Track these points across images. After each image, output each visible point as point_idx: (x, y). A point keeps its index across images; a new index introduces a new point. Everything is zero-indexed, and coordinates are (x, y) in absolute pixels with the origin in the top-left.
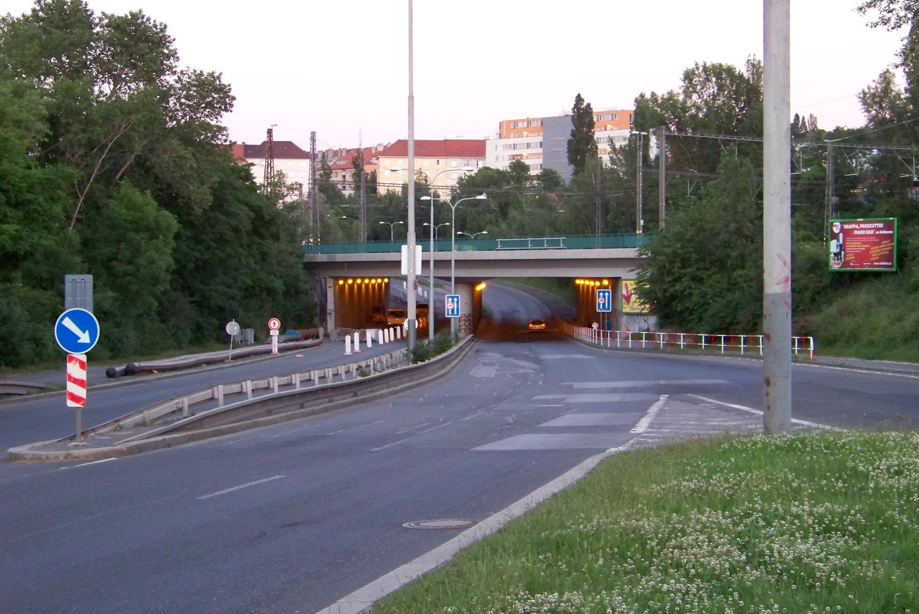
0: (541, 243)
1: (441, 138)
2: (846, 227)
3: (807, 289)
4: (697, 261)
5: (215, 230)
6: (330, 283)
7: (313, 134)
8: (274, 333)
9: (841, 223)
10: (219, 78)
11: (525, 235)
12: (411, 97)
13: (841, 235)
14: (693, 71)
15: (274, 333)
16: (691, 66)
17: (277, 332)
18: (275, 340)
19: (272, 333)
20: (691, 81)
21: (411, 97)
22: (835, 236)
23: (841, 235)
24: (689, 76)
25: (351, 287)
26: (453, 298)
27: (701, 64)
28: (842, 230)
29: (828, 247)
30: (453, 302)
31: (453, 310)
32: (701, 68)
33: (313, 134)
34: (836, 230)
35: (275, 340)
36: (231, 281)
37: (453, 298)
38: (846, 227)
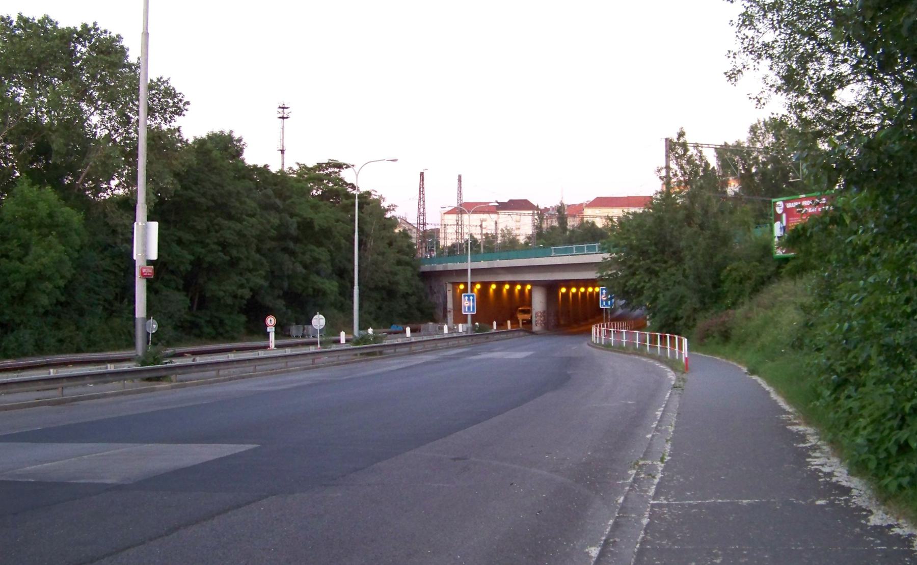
0: (582, 249)
1: (626, 195)
2: (789, 205)
3: (750, 279)
4: (655, 253)
5: (218, 235)
6: (450, 287)
7: (460, 177)
8: (271, 330)
9: (785, 202)
10: (167, 82)
11: (572, 243)
12: (146, 35)
13: (784, 216)
14: (756, 126)
15: (271, 330)
16: (755, 122)
17: (273, 328)
18: (272, 336)
19: (269, 329)
20: (755, 133)
21: (146, 35)
22: (778, 218)
23: (784, 216)
24: (753, 129)
25: (584, 294)
26: (469, 296)
27: (762, 120)
28: (786, 210)
29: (772, 231)
30: (469, 300)
31: (469, 308)
32: (762, 124)
33: (460, 177)
34: (779, 210)
35: (272, 336)
36: (244, 281)
37: (469, 296)
38: (789, 205)
